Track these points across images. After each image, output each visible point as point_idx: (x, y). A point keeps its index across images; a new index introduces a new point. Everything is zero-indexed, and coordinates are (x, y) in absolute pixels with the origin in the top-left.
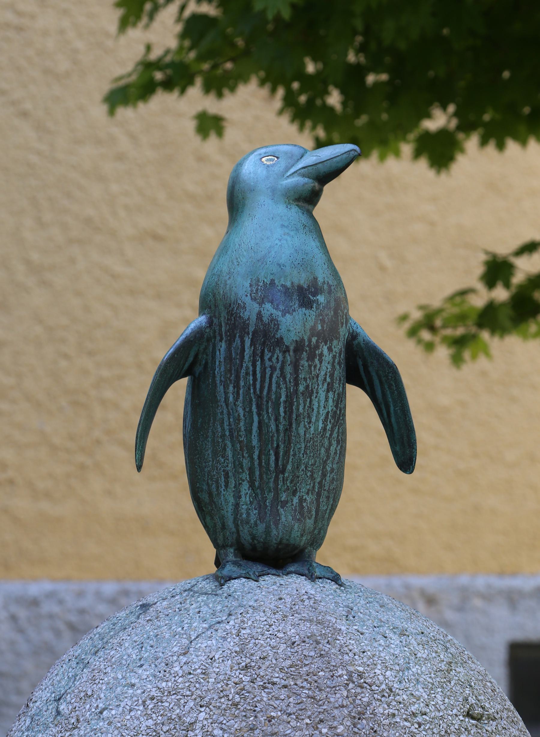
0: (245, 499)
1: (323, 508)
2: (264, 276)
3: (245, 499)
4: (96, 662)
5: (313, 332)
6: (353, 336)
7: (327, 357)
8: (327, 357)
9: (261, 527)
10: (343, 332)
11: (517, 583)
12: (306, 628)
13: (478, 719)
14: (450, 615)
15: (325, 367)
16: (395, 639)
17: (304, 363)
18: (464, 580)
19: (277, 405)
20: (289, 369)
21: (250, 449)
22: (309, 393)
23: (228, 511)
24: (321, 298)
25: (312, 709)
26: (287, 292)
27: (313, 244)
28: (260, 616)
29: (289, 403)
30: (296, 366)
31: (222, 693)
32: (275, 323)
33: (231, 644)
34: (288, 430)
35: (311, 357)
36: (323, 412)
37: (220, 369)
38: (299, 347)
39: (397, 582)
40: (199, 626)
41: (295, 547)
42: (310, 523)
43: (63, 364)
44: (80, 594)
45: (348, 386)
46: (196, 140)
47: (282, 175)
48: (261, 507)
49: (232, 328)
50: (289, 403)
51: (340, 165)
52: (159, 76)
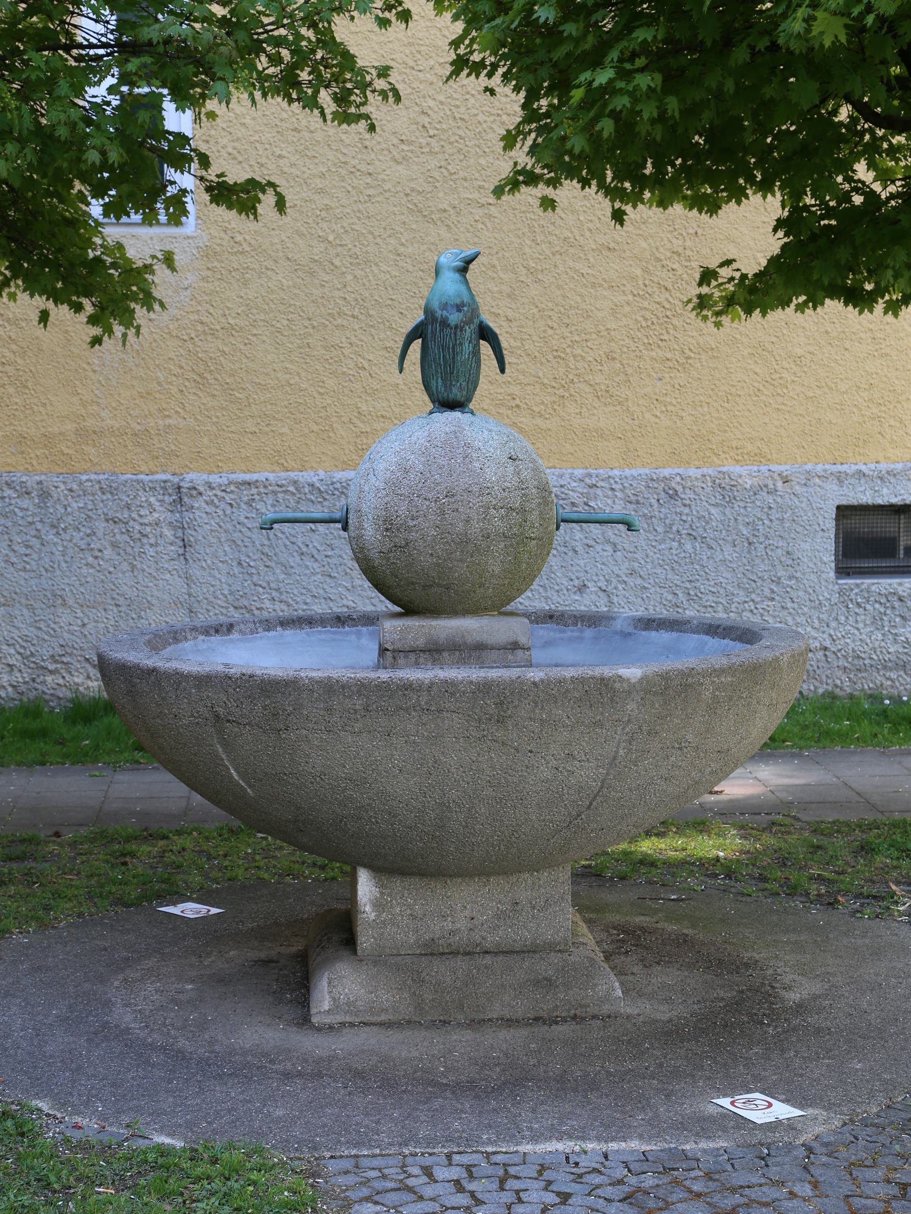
0: (440, 384)
1: (470, 387)
2: (444, 301)
3: (440, 384)
4: (384, 441)
5: (462, 321)
6: (481, 322)
7: (468, 330)
8: (468, 330)
9: (446, 394)
10: (476, 321)
11: (844, 468)
12: (453, 428)
13: (514, 460)
14: (798, 489)
15: (468, 334)
16: (486, 433)
17: (459, 333)
18: (809, 467)
19: (449, 349)
20: (453, 335)
21: (441, 365)
22: (461, 344)
23: (434, 388)
24: (465, 309)
25: (450, 454)
26: (452, 306)
27: (463, 288)
28: (438, 425)
29: (453, 348)
30: (455, 334)
31: (420, 450)
32: (447, 318)
33: (426, 434)
34: (453, 358)
35: (461, 330)
36: (467, 352)
37: (429, 336)
38: (456, 327)
39: (764, 469)
40: (417, 428)
41: (459, 402)
42: (465, 393)
43: (550, 332)
44: (561, 476)
45: (482, 342)
46: (540, 211)
47: (453, 261)
48: (446, 387)
49: (433, 320)
50: (453, 348)
51: (470, 257)
52: (521, 178)
